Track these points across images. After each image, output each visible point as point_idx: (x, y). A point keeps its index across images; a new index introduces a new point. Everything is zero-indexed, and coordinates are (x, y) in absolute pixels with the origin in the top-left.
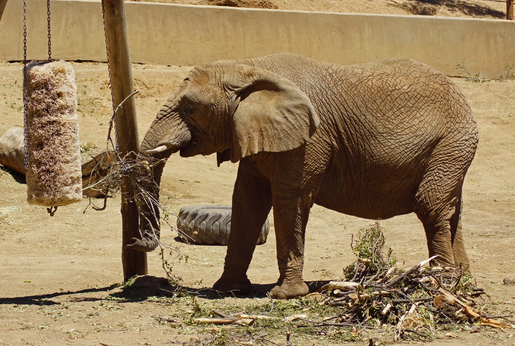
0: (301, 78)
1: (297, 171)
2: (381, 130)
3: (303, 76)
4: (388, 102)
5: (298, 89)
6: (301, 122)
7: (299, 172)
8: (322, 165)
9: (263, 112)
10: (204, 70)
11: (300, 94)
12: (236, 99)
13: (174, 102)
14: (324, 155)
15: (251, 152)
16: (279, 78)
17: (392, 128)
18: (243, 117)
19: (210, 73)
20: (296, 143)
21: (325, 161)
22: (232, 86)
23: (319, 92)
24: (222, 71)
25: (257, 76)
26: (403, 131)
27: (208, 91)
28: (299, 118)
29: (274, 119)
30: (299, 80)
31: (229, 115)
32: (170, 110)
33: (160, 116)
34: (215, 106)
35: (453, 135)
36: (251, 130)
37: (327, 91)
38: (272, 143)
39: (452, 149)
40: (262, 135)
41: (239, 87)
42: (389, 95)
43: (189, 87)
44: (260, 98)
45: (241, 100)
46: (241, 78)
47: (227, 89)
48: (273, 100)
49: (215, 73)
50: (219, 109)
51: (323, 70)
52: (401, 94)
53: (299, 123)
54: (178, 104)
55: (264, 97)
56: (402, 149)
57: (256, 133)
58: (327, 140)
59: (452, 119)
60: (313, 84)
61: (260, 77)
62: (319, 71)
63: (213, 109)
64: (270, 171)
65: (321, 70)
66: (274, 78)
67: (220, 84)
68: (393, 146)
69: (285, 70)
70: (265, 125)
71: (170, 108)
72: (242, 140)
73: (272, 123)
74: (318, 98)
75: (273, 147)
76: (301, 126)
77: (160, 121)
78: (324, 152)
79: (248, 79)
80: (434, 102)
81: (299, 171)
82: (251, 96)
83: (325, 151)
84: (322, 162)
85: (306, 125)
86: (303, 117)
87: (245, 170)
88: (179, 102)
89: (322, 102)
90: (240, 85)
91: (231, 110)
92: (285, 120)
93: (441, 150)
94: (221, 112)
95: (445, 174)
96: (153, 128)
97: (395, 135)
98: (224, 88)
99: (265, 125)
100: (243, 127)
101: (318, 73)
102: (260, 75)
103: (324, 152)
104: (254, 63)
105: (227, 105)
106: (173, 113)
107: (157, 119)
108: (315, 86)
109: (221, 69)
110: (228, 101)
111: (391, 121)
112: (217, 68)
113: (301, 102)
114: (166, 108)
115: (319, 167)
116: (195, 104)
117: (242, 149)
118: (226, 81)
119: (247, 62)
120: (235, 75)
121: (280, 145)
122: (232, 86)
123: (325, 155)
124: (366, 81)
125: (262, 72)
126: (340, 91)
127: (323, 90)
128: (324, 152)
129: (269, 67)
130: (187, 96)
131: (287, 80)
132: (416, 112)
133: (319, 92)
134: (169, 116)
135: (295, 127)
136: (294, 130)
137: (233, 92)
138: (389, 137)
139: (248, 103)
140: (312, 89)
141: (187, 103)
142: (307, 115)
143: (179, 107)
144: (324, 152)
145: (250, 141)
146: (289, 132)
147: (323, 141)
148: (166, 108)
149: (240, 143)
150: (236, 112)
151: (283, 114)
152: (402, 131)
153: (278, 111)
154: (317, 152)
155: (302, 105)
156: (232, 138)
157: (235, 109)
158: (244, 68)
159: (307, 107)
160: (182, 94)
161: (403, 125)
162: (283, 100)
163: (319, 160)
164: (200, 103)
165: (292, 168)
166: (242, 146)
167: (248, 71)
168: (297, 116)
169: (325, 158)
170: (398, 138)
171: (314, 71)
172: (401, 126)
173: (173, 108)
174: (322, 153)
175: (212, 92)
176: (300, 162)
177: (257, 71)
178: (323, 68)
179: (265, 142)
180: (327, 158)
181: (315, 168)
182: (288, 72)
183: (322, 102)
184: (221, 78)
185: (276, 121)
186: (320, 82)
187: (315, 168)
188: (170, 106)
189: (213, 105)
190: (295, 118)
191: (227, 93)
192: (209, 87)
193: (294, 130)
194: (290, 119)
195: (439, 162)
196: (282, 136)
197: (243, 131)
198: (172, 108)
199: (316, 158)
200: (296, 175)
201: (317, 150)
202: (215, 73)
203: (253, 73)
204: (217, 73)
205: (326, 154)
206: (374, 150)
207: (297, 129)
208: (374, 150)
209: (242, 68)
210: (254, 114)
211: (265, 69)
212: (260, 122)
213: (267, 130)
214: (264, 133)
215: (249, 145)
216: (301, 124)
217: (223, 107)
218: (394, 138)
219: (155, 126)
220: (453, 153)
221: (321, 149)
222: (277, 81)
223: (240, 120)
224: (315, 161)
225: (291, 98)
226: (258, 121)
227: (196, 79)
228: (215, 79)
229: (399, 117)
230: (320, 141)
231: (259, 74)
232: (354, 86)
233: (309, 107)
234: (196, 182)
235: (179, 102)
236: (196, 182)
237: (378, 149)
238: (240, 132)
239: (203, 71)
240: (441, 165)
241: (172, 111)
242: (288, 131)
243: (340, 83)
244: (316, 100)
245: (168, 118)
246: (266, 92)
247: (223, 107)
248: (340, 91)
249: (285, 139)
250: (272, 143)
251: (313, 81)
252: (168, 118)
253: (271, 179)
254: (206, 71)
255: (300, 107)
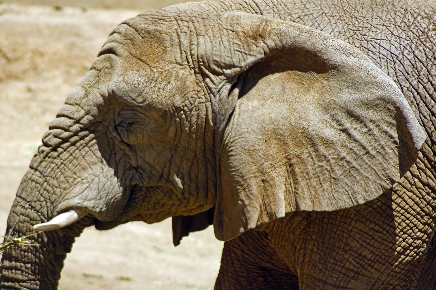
0: (369, 39)
1: (360, 255)
3: (373, 35)
5: (371, 65)
6: (381, 139)
7: (364, 257)
8: (418, 242)
9: (293, 120)
10: (151, 28)
11: (375, 73)
12: (229, 94)
13: (86, 108)
14: (422, 217)
15: (271, 215)
16: (324, 39)
18: (247, 135)
19: (166, 37)
20: (372, 187)
21: (425, 232)
22: (218, 65)
23: (411, 70)
24: (193, 29)
25: (273, 37)
27: (167, 78)
28: (376, 131)
29: (318, 135)
30: (364, 43)
31: (215, 132)
32: (76, 127)
33: (55, 141)
34: (185, 112)
36: (266, 165)
37: (429, 67)
38: (316, 191)
40: (293, 173)
41: (234, 66)
43: (118, 70)
44: (284, 89)
45: (241, 95)
46: (239, 45)
47: (207, 72)
48: (312, 92)
49: (178, 35)
50: (194, 119)
51: (419, 18)
53: (377, 141)
54: (95, 111)
55: (291, 85)
57: (278, 170)
58: (430, 181)
60: (397, 53)
61: (281, 41)
62: (412, 20)
63: (181, 118)
64: (297, 254)
65: (415, 19)
66: (314, 40)
67: (190, 61)
69: (333, 21)
70: (298, 151)
71: (77, 121)
72: (247, 188)
73: (314, 145)
74: (408, 85)
75: (320, 201)
76: (383, 147)
77: (55, 154)
78: (422, 209)
79: (254, 47)
81: (364, 253)
82: (262, 83)
83: (425, 209)
84: (418, 234)
85: (393, 146)
86: (385, 127)
87: (239, 252)
88: (98, 106)
89: (419, 93)
90: (236, 61)
91: (218, 121)
92: (344, 135)
94: (197, 125)
96: (39, 168)
98: (200, 69)
99: (298, 151)
100: (247, 158)
101: (409, 27)
102: (280, 35)
103: (424, 211)
104: (262, 8)
105: (210, 109)
106: (87, 132)
107: (47, 149)
108: (401, 57)
109: (191, 24)
110: (213, 99)
112: (180, 22)
113: (379, 93)
114: (68, 122)
115: (410, 245)
116: (139, 109)
117: (249, 208)
118: (203, 53)
119: (245, 5)
120: (225, 38)
121: (336, 195)
122: (218, 65)
123: (426, 218)
125: (284, 27)
127: (419, 65)
128: (422, 209)
129: (296, 16)
130: (117, 92)
131: (344, 43)
133: (410, 69)
134: (77, 141)
135: (368, 152)
136: (365, 157)
137: (223, 77)
139: (256, 102)
140: (395, 63)
141: (117, 110)
142: (394, 122)
143: (99, 120)
144: (424, 211)
145: (265, 189)
146: (355, 164)
147: (420, 185)
148: (68, 122)
149: (242, 195)
150: (231, 124)
151: (339, 123)
153: (326, 117)
154: (406, 211)
155: (383, 99)
156: (220, 184)
157: (227, 117)
158: (243, 21)
159: (393, 104)
160: (105, 88)
162: (337, 90)
163: (411, 228)
164: (151, 107)
165: (348, 248)
166: (247, 202)
167: (252, 26)
168: (372, 126)
169: (424, 224)
171: (399, 20)
173: (85, 121)
174: (419, 214)
175: (176, 80)
176: (366, 233)
177: (274, 26)
178: (419, 14)
179: (300, 189)
180: (429, 225)
181: (403, 248)
182: (341, 27)
183: (419, 93)
184: (193, 47)
185: (322, 139)
186: (413, 46)
187: (403, 248)
188: (77, 116)
189: (178, 109)
190: (366, 130)
191: (208, 80)
192: (166, 68)
193: (365, 157)
194: (354, 134)
196: (339, 173)
197: (248, 167)
198: (82, 121)
199: (404, 225)
200: (358, 263)
201: (407, 207)
202: (178, 35)
203: (264, 30)
204: (182, 35)
205: (427, 214)
207: (373, 157)
209: (237, 19)
210: (272, 127)
211: (288, 19)
212: (286, 144)
213: (302, 162)
214: (297, 170)
215: (263, 200)
216: (383, 143)
217: (203, 113)
219: (44, 164)
221: (416, 203)
222: (320, 47)
223: (240, 142)
224: (402, 231)
226: (282, 142)
227: (134, 52)
228: (178, 50)
230: (415, 184)
231: (278, 32)
233: (398, 105)
234: (122, 279)
235: (98, 106)
236: (122, 279)
238: (242, 171)
239: (148, 32)
241: (82, 130)
242: (352, 161)
244: (405, 89)
245: (74, 144)
246: (296, 74)
247: (203, 113)
249: (347, 181)
250: (316, 191)
251: (397, 45)
252: (74, 144)
253: (299, 272)
254: (156, 30)
255: (376, 105)
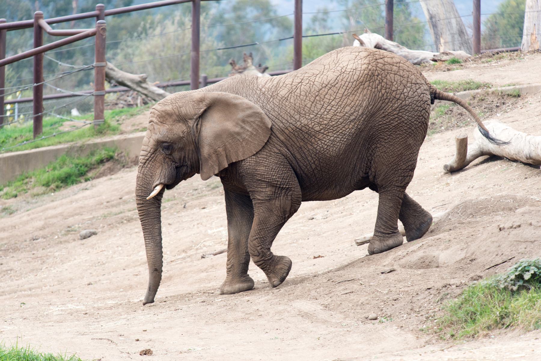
2: (317, 129)
4: (318, 102)
17: (327, 122)
26: (338, 121)
35: (391, 105)
39: (391, 118)
42: (317, 96)
52: (329, 90)
56: (340, 137)
59: (387, 90)
68: (332, 138)
80: (363, 84)
93: (380, 121)
95: (386, 141)
97: (332, 128)
109: (177, 104)
111: (325, 117)
124: (295, 90)
126: (273, 107)
132: (346, 100)
138: (327, 132)
152: (337, 123)
161: (336, 116)
170: (334, 129)
172: (335, 118)
173: (151, 151)
195: (379, 132)
206: (317, 147)
208: (317, 147)
218: (331, 131)
220: (392, 122)
225: (243, 110)
229: (331, 111)
232: (284, 98)
237: (321, 146)
240: (381, 133)
243: (272, 99)
248: (273, 107)
